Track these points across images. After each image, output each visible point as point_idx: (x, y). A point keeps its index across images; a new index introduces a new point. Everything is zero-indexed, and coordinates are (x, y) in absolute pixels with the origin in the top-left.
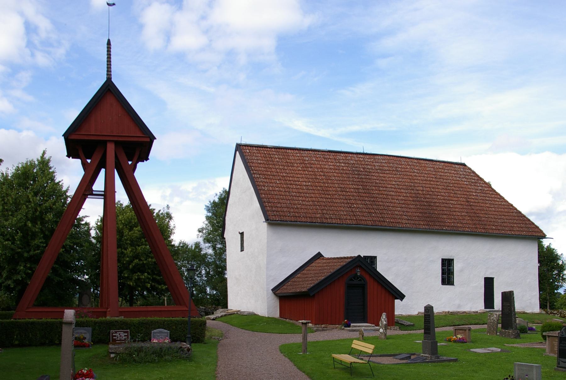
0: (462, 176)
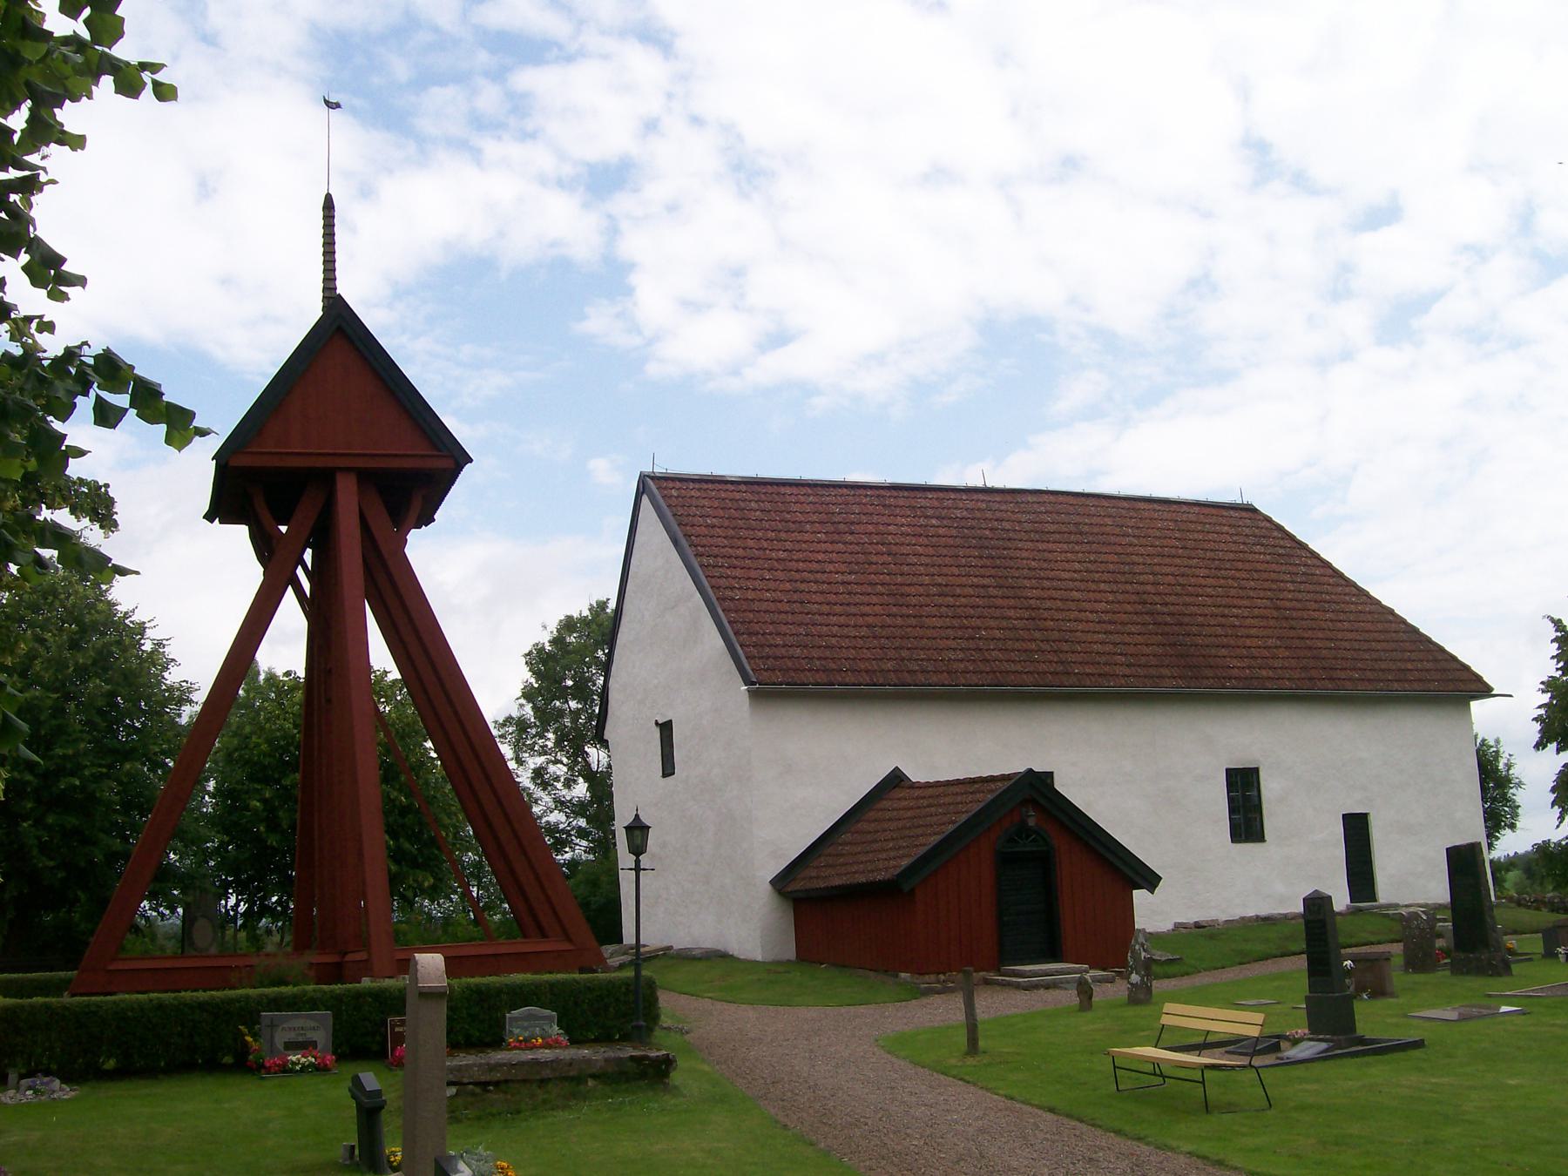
0: (1251, 540)
